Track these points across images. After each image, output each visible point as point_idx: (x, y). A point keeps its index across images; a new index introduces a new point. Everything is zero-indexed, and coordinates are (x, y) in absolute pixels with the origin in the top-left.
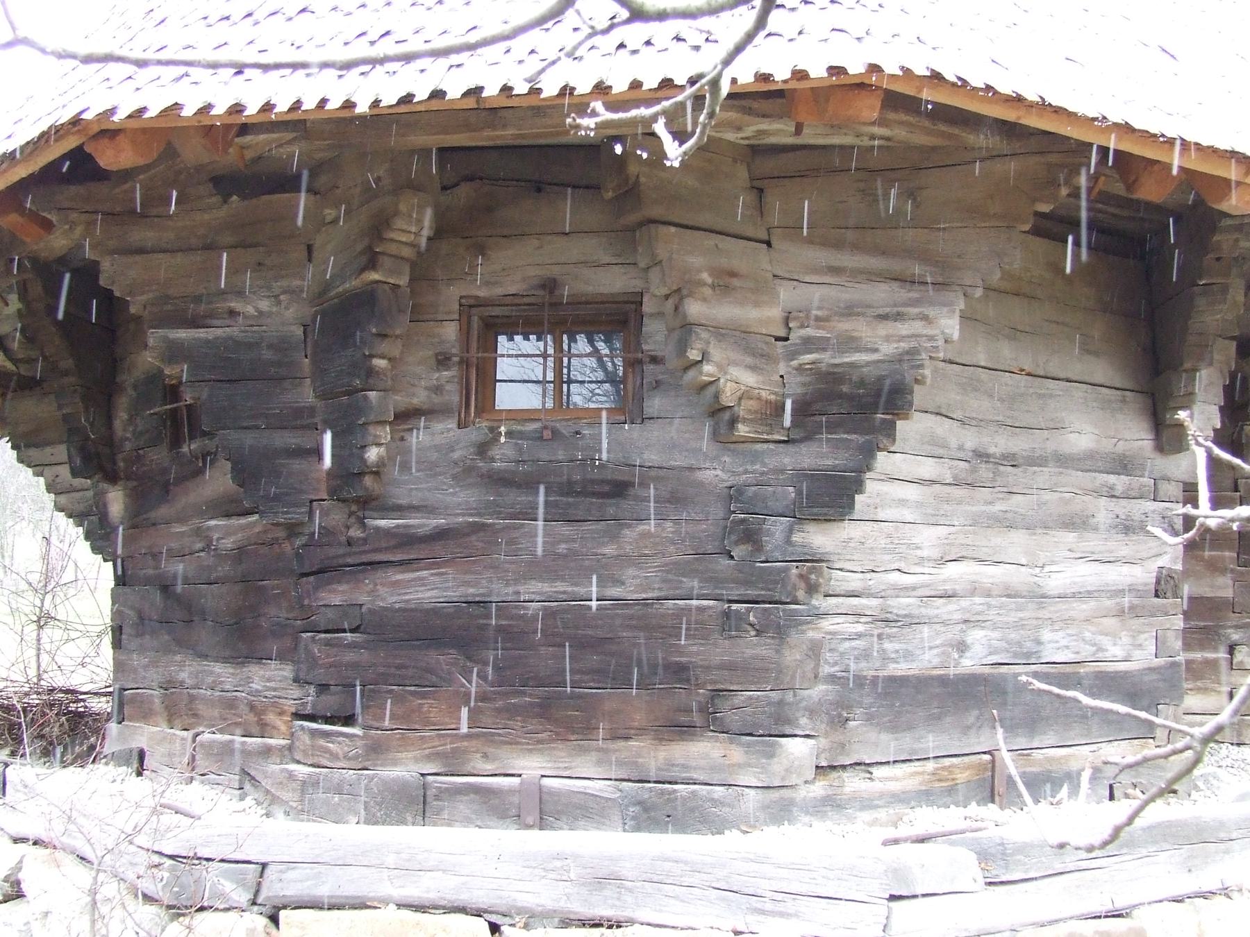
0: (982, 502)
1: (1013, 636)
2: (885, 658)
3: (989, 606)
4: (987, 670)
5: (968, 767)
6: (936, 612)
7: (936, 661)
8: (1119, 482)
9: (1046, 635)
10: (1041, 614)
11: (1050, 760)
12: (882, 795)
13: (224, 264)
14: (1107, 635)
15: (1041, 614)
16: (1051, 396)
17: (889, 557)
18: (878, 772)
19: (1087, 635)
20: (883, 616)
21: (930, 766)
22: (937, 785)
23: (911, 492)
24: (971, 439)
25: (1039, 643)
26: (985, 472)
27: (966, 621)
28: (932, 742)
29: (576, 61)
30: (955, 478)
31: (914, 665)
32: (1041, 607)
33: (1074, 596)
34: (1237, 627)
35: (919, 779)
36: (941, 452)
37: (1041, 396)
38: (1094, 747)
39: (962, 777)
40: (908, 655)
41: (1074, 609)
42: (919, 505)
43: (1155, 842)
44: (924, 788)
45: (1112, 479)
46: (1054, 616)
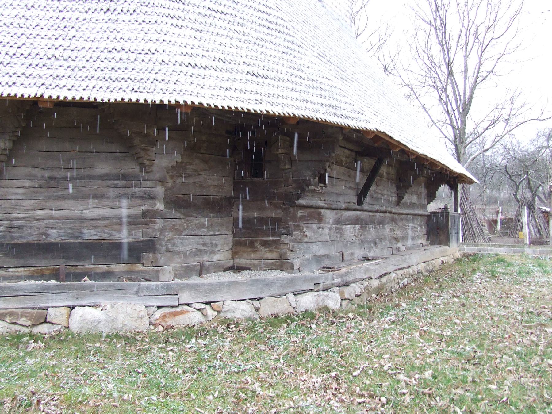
0: (52, 192)
1: (70, 231)
2: (13, 238)
3: (58, 223)
4: (58, 241)
5: (49, 269)
6: (34, 225)
7: (35, 239)
8: (120, 183)
9: (85, 231)
10: (82, 225)
11: (87, 268)
12: (13, 276)
13: (98, 121)
14: (115, 231)
15: (82, 225)
16: (89, 158)
17: (12, 209)
18: (10, 270)
19: (106, 231)
20: (10, 226)
21: (33, 269)
22: (36, 274)
23: (21, 191)
24: (47, 174)
25: (82, 233)
26: (53, 183)
27: (47, 227)
28: (34, 262)
29: (366, 7)
30: (39, 186)
31: (26, 240)
32: (81, 222)
33: (100, 219)
34: (284, 228)
35: (29, 272)
36: (34, 178)
37: (83, 158)
38: (108, 266)
39: (48, 272)
40: (22, 237)
41: (98, 223)
42: (23, 194)
43: (60, 290)
44: (30, 275)
45: (116, 182)
46: (89, 226)
